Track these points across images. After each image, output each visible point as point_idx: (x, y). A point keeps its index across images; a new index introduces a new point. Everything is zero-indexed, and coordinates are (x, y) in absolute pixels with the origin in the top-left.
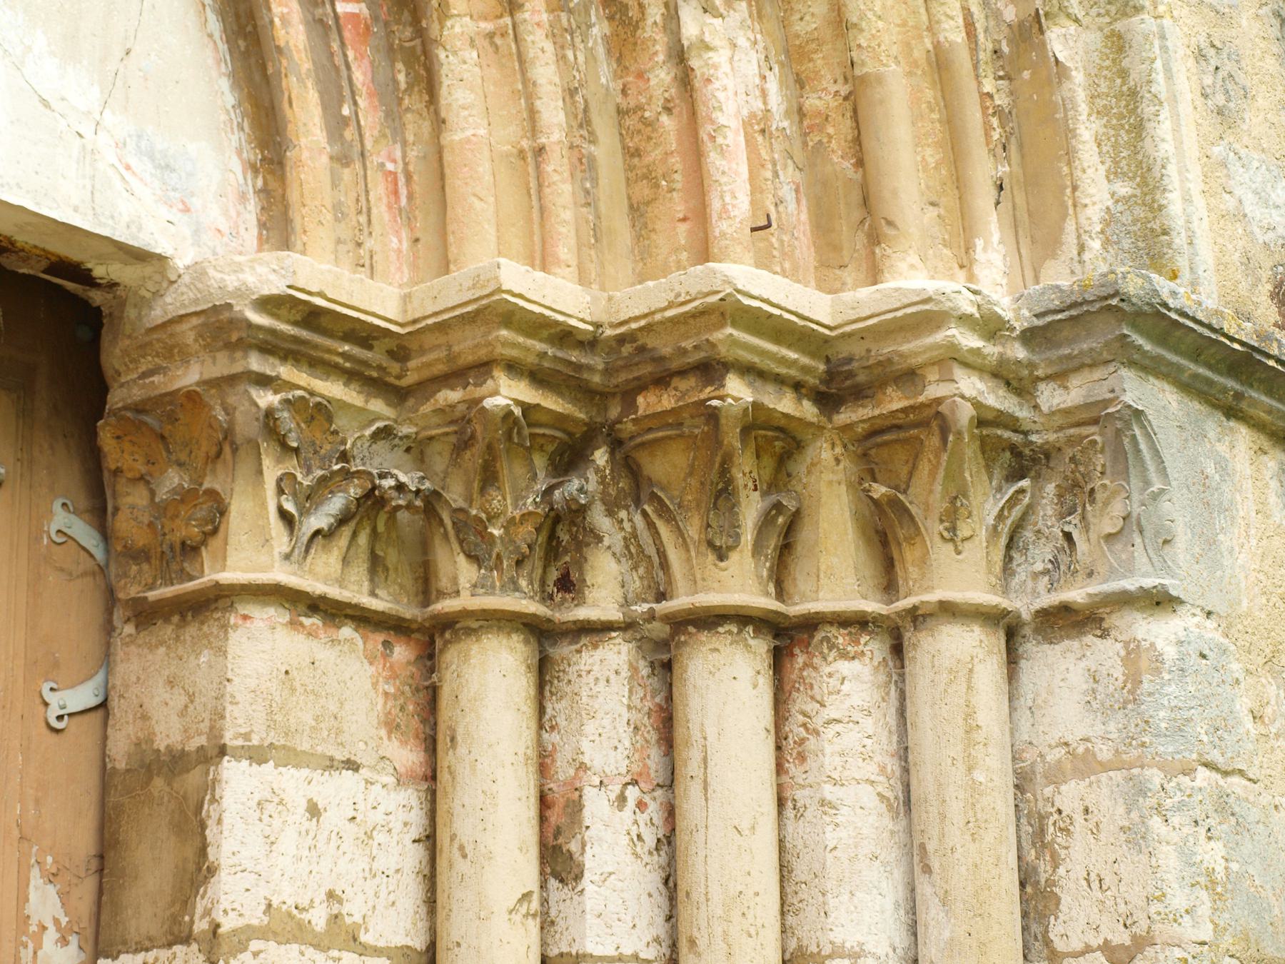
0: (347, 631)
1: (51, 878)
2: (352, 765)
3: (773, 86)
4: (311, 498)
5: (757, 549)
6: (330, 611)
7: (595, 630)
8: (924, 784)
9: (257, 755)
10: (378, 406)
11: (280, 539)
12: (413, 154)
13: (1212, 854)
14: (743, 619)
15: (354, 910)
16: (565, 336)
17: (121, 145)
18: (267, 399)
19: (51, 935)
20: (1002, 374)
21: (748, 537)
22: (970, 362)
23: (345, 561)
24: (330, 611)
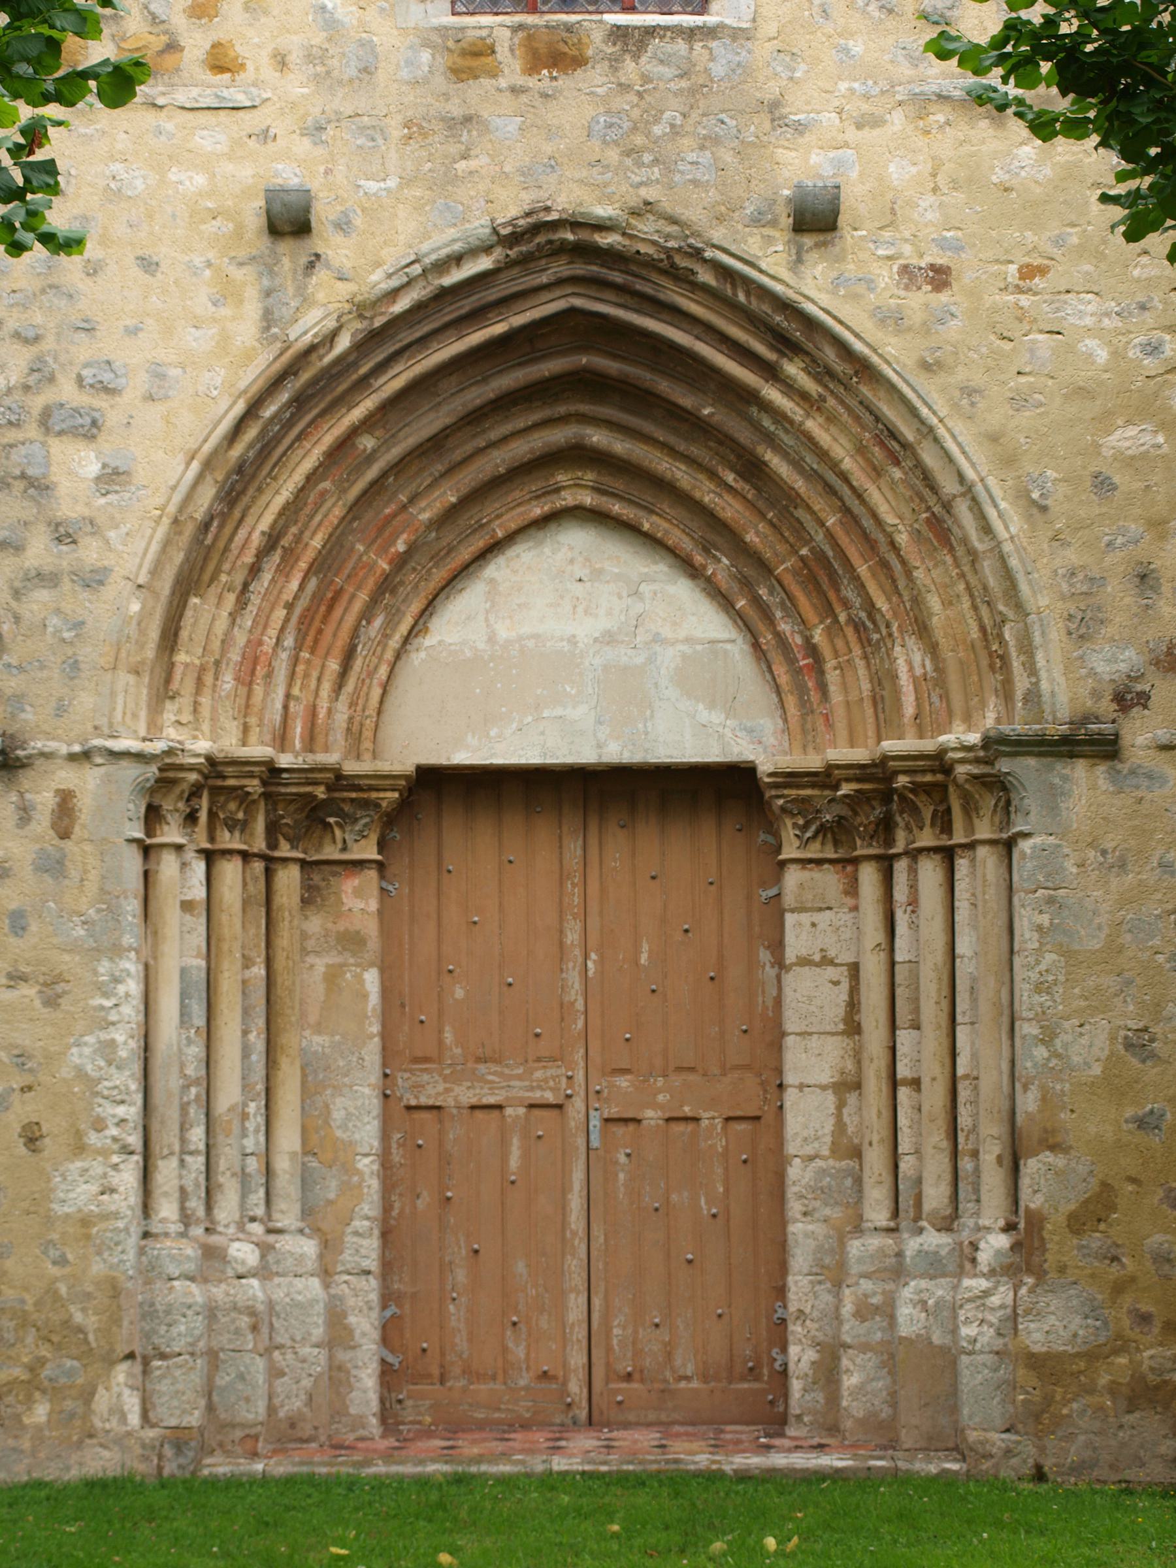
0: (826, 866)
1: (768, 948)
2: (830, 908)
3: (928, 663)
4: (804, 828)
5: (933, 825)
6: (819, 862)
7: (897, 856)
8: (1004, 894)
9: (793, 911)
10: (827, 792)
11: (797, 843)
12: (352, 961)
13: (1045, 919)
14: (928, 850)
15: (832, 953)
16: (863, 766)
17: (733, 730)
18: (781, 802)
19: (768, 965)
20: (977, 761)
21: (928, 822)
22: (962, 761)
23: (823, 844)
24: (819, 862)
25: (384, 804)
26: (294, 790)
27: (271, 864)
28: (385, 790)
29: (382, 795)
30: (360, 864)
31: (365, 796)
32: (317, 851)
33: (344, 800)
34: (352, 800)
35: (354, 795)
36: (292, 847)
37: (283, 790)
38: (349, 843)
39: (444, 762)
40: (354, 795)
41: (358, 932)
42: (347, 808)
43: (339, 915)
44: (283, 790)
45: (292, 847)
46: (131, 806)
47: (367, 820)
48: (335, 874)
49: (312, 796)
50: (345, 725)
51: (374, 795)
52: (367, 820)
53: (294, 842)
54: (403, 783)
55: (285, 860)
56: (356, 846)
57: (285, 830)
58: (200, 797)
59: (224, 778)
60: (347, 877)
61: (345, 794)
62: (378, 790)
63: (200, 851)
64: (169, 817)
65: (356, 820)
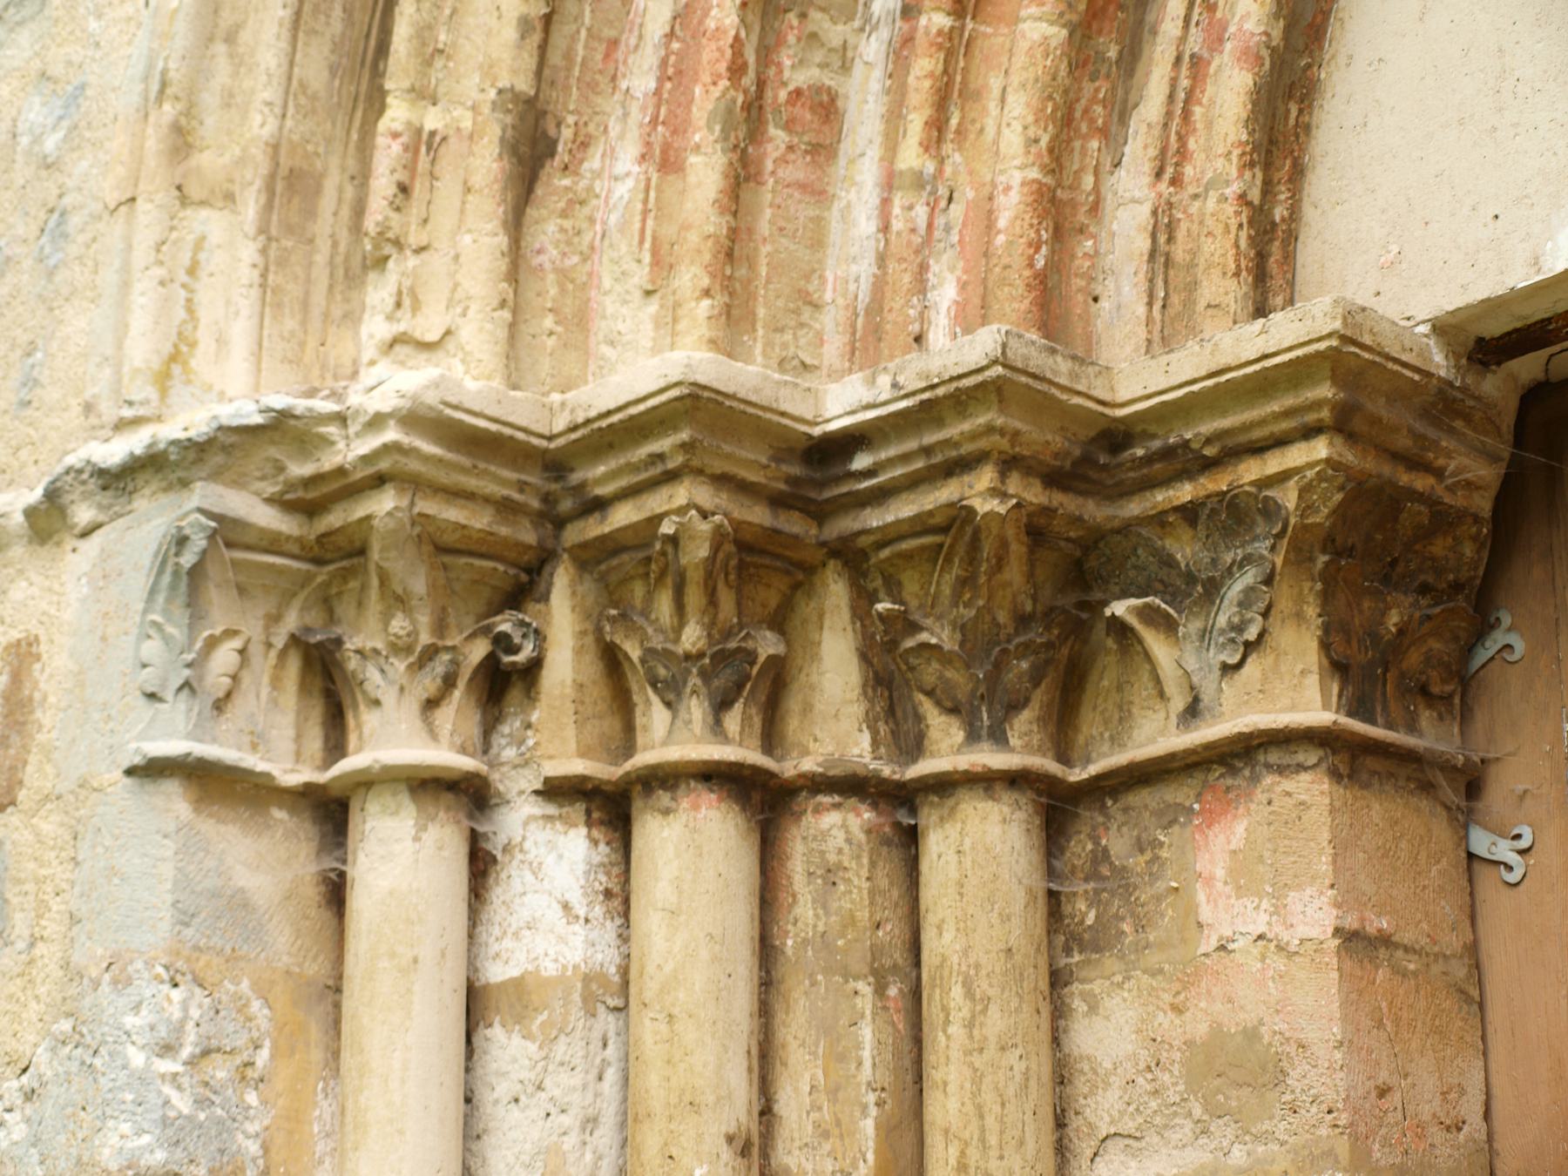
25: (1289, 497)
26: (903, 509)
27: (901, 809)
28: (1281, 442)
29: (1274, 463)
30: (1243, 754)
31: (1218, 483)
32: (1117, 742)
33: (1159, 520)
34: (1189, 513)
35: (1185, 492)
36: (973, 737)
37: (875, 518)
38: (1208, 685)
39: (1522, 278)
40: (1185, 492)
41: (1251, 1034)
42: (1185, 549)
43: (1189, 977)
44: (875, 518)
45: (973, 737)
46: (152, 649)
47: (1249, 577)
48: (1171, 816)
49: (958, 518)
50: (1144, 244)
51: (1250, 471)
52: (1249, 577)
53: (986, 713)
54: (1325, 391)
55: (944, 785)
56: (1231, 690)
57: (930, 672)
58: (545, 598)
59: (599, 505)
60: (1211, 818)
61: (1162, 498)
62: (1258, 449)
63: (557, 791)
64: (373, 675)
65: (1213, 589)
